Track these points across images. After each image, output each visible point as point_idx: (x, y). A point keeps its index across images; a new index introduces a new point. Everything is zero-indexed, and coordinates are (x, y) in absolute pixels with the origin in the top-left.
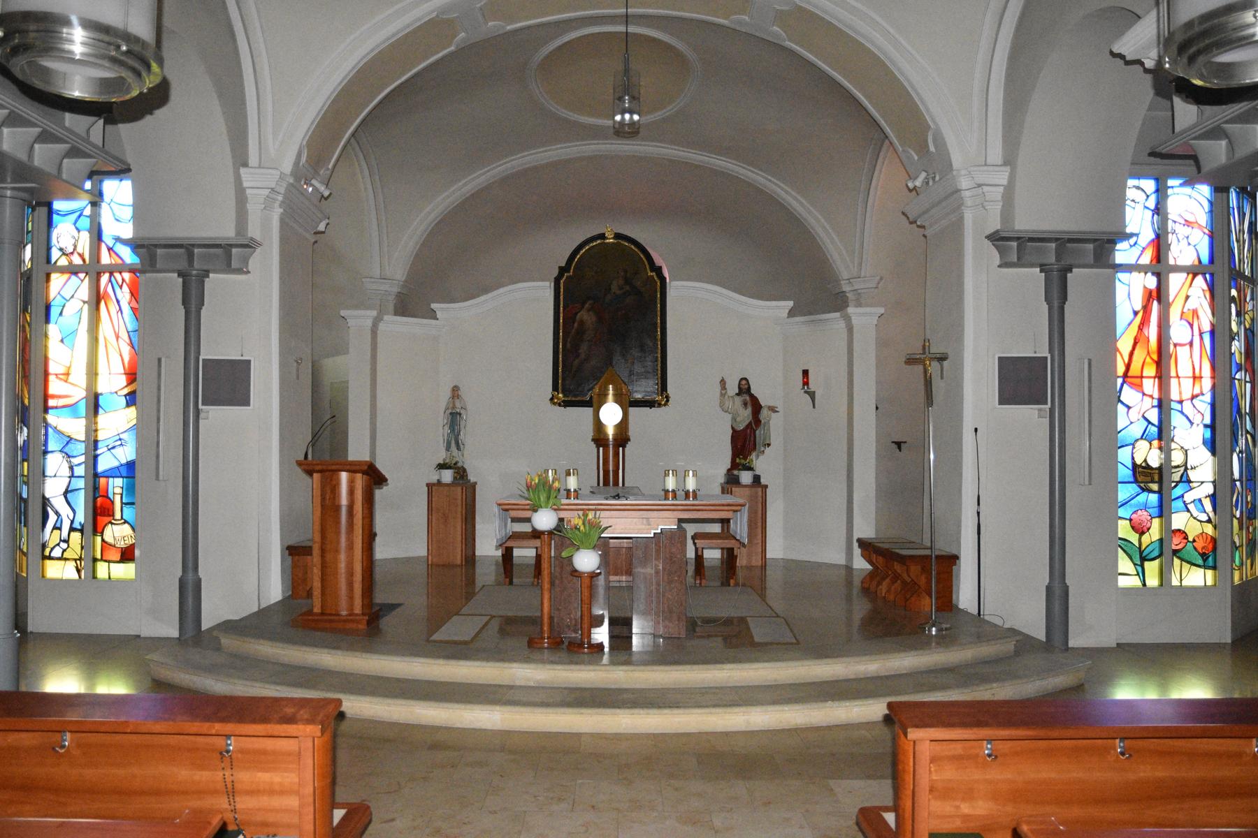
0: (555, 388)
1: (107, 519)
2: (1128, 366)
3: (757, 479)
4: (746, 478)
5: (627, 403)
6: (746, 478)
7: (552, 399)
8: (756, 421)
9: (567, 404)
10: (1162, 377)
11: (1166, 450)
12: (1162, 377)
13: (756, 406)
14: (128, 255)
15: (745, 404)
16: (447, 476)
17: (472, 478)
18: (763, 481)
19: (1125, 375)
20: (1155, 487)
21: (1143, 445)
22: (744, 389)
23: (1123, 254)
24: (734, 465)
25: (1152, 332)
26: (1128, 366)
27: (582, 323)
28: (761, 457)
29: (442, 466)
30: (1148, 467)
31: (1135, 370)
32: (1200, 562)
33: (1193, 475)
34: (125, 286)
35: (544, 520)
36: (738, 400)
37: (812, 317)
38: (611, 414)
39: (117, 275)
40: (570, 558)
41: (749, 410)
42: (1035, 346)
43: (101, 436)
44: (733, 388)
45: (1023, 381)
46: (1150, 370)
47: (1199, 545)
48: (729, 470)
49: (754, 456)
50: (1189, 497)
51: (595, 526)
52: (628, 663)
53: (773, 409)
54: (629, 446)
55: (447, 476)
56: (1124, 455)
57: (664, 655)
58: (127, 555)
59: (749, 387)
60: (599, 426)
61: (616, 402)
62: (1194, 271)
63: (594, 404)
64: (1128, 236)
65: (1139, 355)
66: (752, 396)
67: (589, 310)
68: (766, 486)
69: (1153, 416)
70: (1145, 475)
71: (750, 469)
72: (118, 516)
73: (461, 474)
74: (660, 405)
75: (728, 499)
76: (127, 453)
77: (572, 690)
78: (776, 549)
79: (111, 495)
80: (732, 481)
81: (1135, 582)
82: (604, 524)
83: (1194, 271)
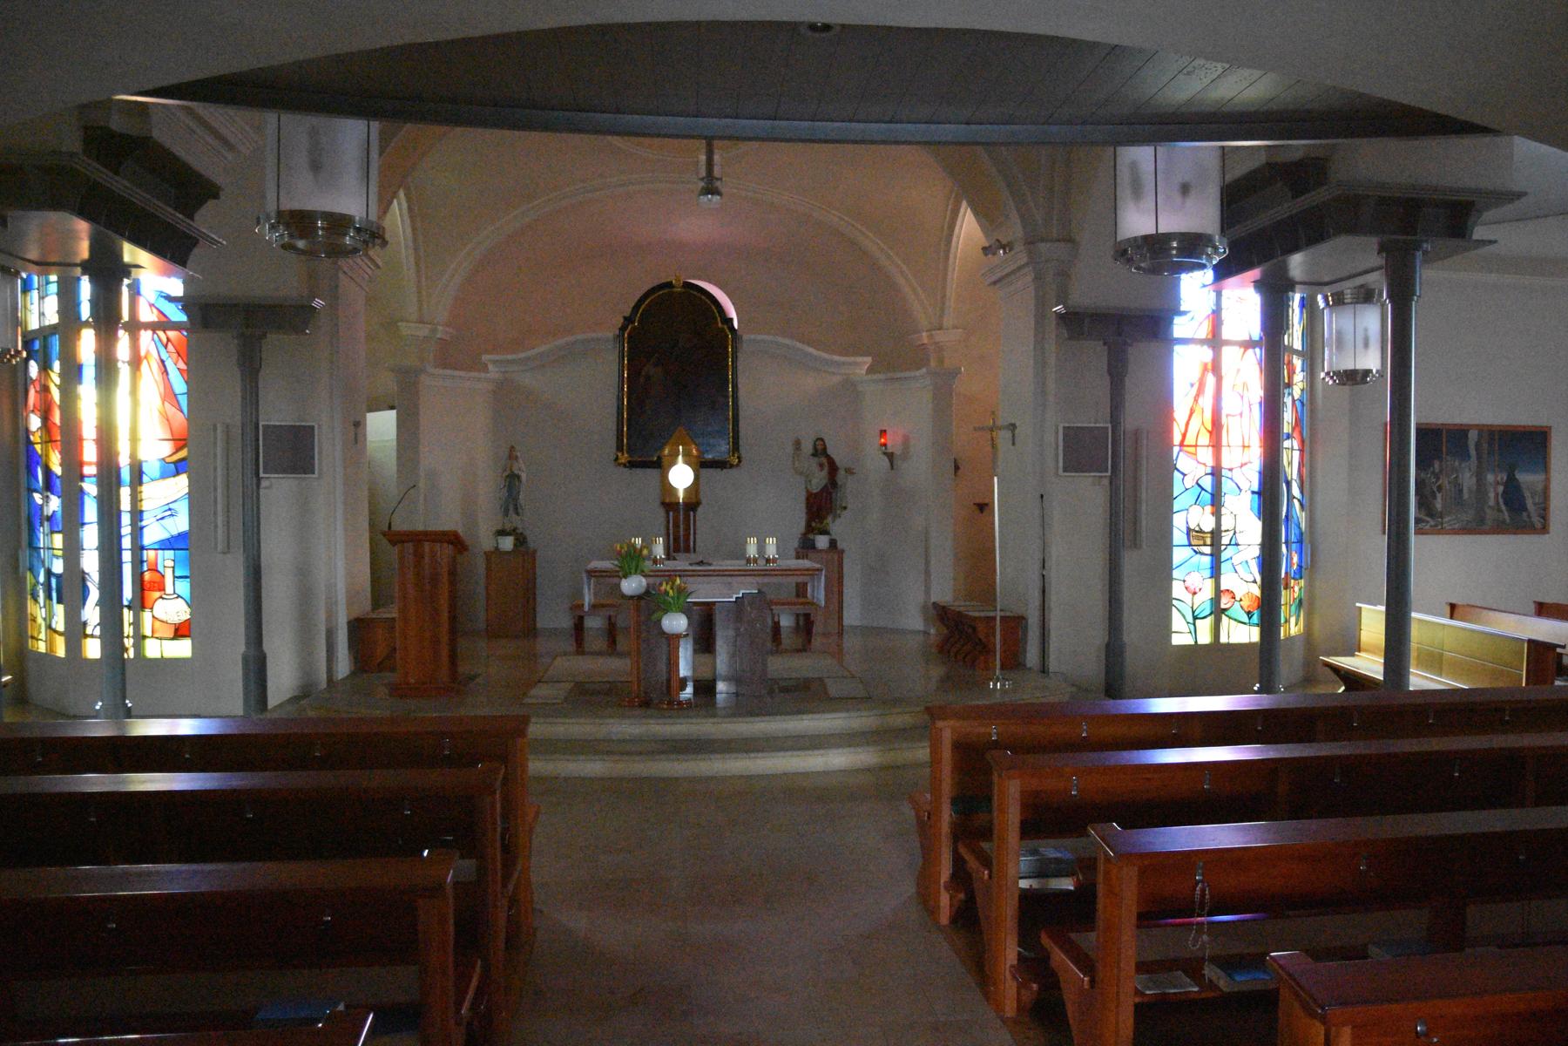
0: (620, 448)
1: (157, 594)
2: (1184, 436)
3: (833, 543)
4: (822, 542)
5: (701, 465)
6: (822, 542)
7: (617, 459)
8: (833, 483)
9: (632, 465)
10: (1216, 445)
11: (1217, 513)
12: (1216, 445)
13: (833, 468)
14: (177, 315)
15: (821, 465)
16: (507, 543)
17: (532, 545)
18: (840, 545)
19: (1182, 445)
20: (1207, 550)
21: (1196, 510)
22: (820, 450)
23: (1180, 327)
24: (809, 529)
25: (1207, 401)
26: (1184, 436)
27: (648, 378)
28: (838, 521)
29: (502, 533)
30: (1201, 531)
31: (1189, 440)
32: (1246, 619)
33: (1240, 539)
34: (170, 346)
35: (632, 585)
36: (814, 462)
37: (890, 375)
38: (681, 476)
39: (161, 333)
40: (659, 621)
41: (825, 473)
42: (1094, 417)
43: (145, 506)
44: (807, 447)
45: (1083, 450)
46: (1205, 439)
47: (1245, 603)
48: (805, 534)
49: (829, 519)
50: (1236, 560)
51: (681, 591)
52: (714, 716)
53: (849, 471)
54: (700, 510)
55: (507, 543)
56: (1179, 522)
57: (744, 706)
58: (180, 632)
59: (825, 449)
60: (669, 489)
61: (686, 462)
62: (1248, 344)
63: (662, 466)
64: (1184, 313)
65: (1195, 424)
66: (828, 457)
67: (656, 365)
68: (843, 551)
69: (1207, 482)
70: (1198, 538)
71: (825, 532)
72: (169, 589)
73: (521, 540)
74: (732, 466)
75: (806, 563)
76: (181, 523)
77: (664, 741)
78: (852, 616)
79: (160, 568)
80: (806, 547)
81: (1189, 641)
82: (690, 588)
83: (1248, 344)
